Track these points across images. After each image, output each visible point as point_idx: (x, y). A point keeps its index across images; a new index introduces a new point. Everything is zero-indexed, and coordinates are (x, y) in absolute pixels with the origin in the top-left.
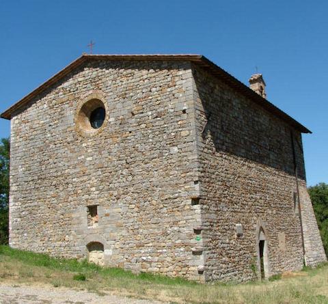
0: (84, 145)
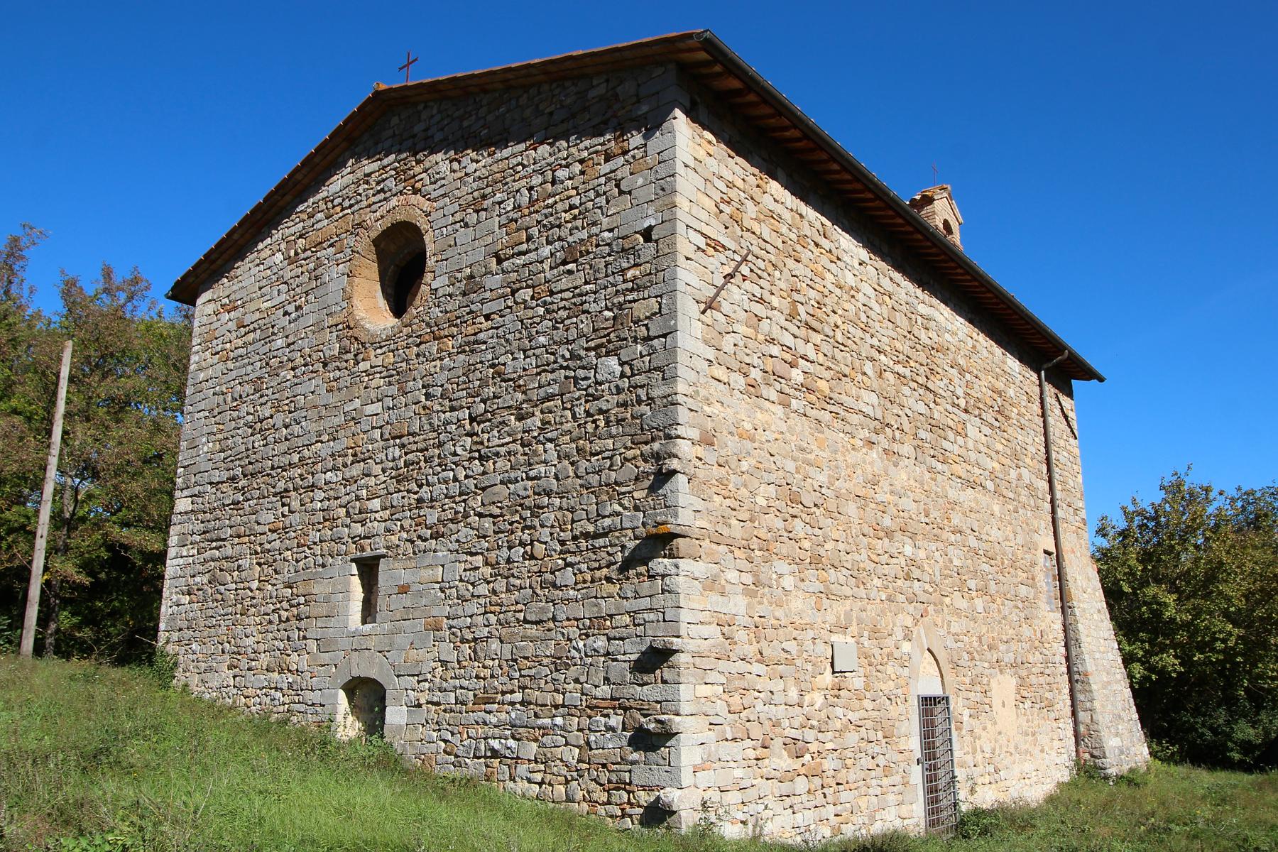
0: (363, 366)
